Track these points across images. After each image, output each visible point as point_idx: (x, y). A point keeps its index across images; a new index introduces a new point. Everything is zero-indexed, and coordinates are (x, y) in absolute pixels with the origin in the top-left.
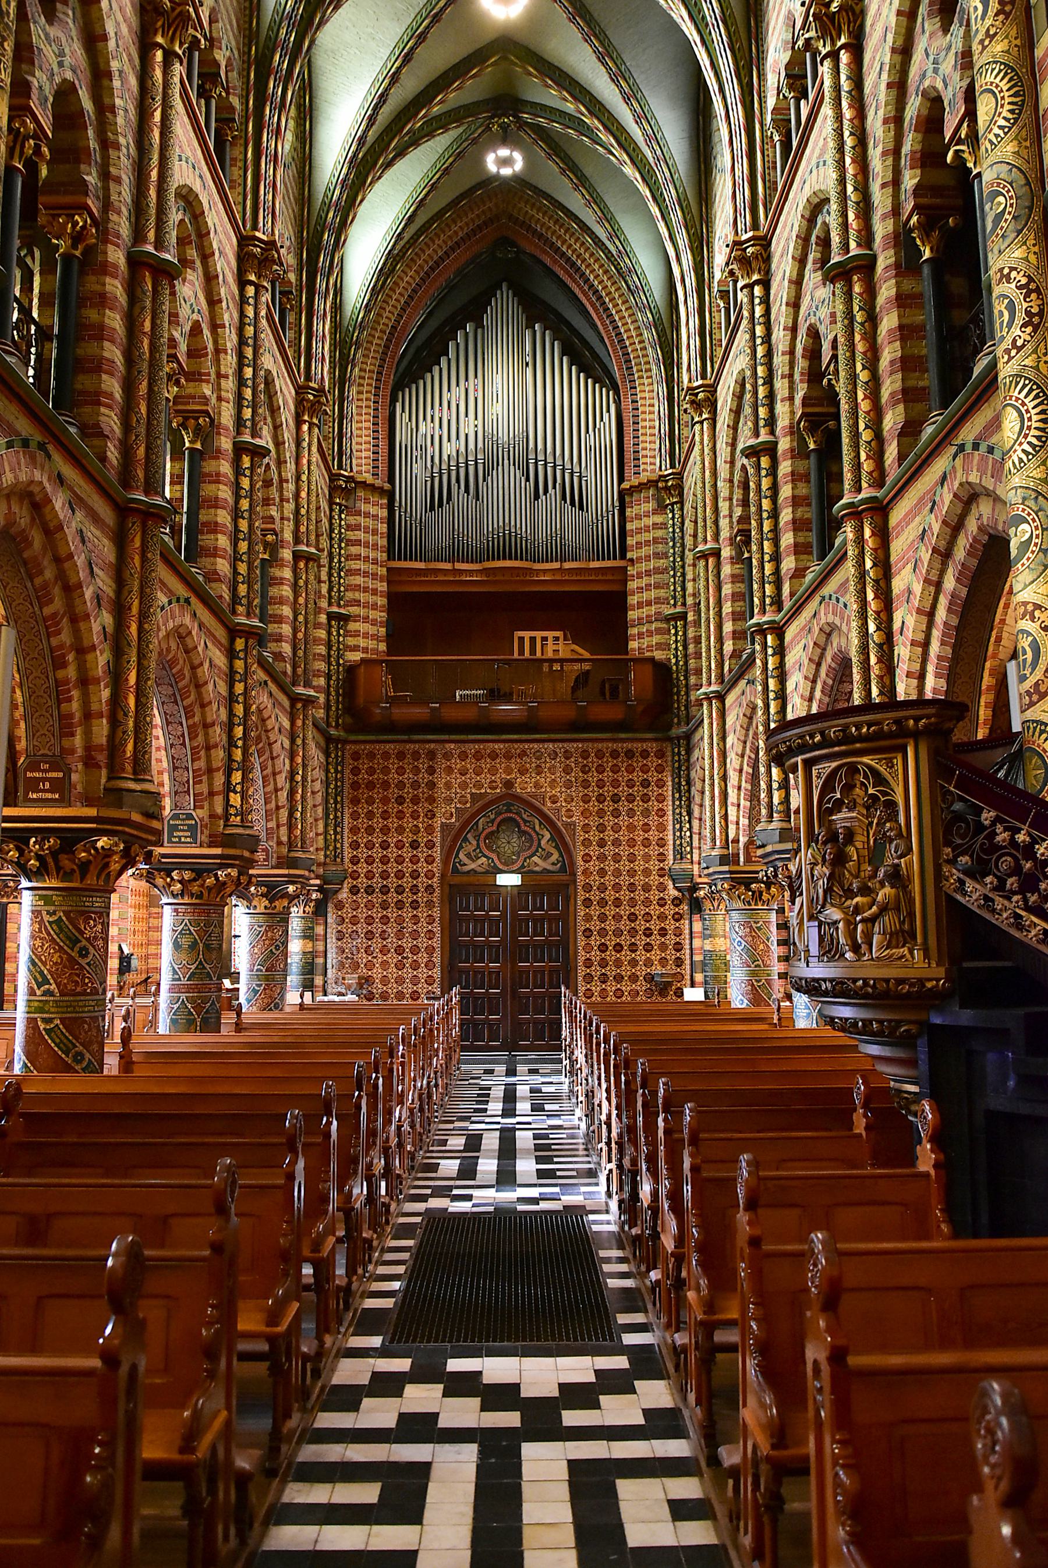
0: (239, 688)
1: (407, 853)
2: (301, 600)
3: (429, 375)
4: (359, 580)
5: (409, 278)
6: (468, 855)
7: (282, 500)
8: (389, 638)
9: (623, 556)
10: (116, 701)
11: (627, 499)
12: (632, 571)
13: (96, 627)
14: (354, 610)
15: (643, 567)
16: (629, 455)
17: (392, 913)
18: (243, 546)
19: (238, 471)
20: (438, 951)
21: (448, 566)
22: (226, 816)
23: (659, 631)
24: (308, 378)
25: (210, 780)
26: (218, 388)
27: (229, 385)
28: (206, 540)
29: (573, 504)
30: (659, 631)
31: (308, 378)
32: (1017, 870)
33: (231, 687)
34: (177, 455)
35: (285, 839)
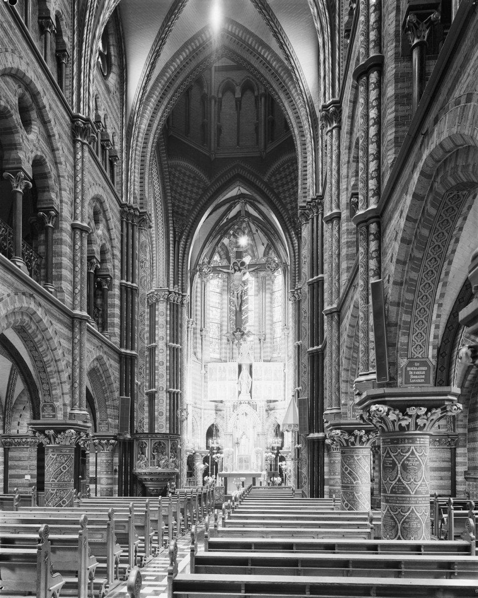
7: (60, 189)
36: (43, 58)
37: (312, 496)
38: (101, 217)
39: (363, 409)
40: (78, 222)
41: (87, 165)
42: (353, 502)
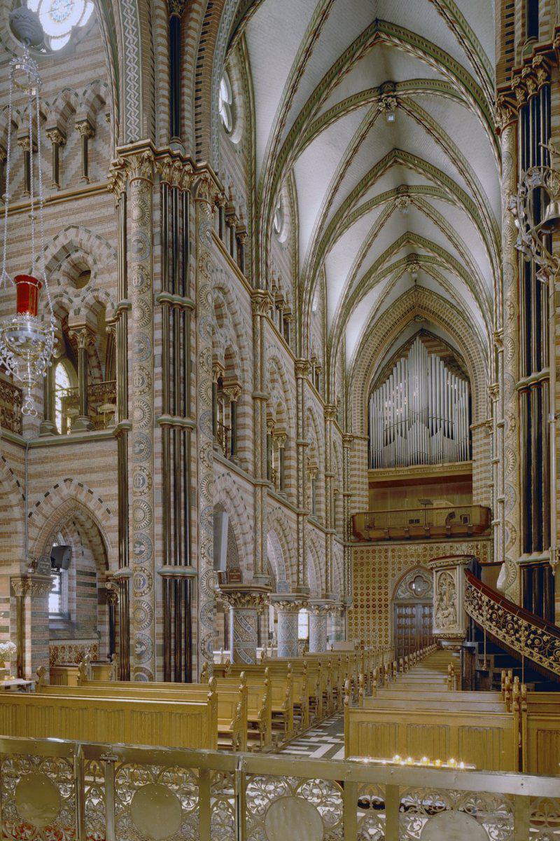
0: (301, 535)
1: (377, 591)
2: (329, 494)
3: (387, 381)
4: (356, 479)
5: (374, 342)
6: (402, 592)
8: (370, 504)
9: (471, 459)
10: (255, 549)
11: (473, 432)
12: (474, 465)
13: (248, 526)
14: (354, 492)
15: (479, 463)
16: (474, 412)
17: (371, 615)
18: (301, 482)
19: (298, 453)
20: (390, 631)
21: (393, 469)
22: (298, 582)
23: (485, 492)
24: (329, 402)
25: (292, 569)
26: (289, 423)
27: (294, 421)
28: (287, 481)
29: (448, 437)
30: (485, 492)
31: (329, 402)
32: (478, 604)
33: (298, 534)
34: (276, 450)
35: (324, 587)
36: (229, 254)
37: (167, 678)
38: (225, 310)
39: (475, 632)
40: (259, 392)
41: (266, 335)
42: (92, 619)
